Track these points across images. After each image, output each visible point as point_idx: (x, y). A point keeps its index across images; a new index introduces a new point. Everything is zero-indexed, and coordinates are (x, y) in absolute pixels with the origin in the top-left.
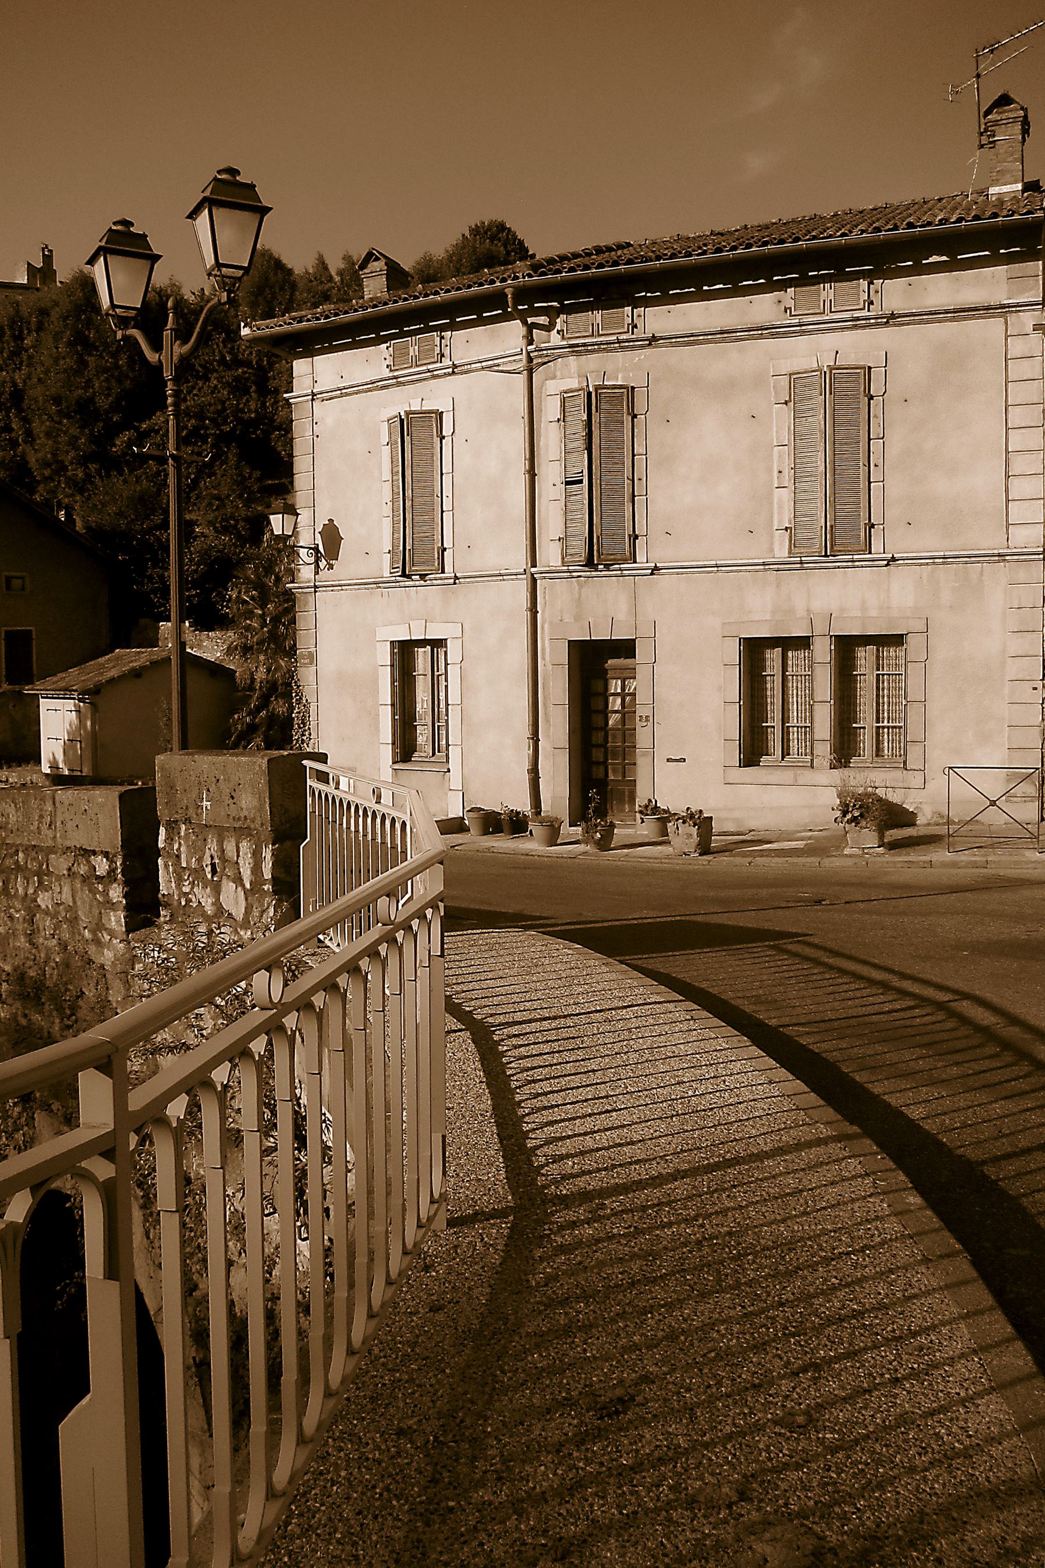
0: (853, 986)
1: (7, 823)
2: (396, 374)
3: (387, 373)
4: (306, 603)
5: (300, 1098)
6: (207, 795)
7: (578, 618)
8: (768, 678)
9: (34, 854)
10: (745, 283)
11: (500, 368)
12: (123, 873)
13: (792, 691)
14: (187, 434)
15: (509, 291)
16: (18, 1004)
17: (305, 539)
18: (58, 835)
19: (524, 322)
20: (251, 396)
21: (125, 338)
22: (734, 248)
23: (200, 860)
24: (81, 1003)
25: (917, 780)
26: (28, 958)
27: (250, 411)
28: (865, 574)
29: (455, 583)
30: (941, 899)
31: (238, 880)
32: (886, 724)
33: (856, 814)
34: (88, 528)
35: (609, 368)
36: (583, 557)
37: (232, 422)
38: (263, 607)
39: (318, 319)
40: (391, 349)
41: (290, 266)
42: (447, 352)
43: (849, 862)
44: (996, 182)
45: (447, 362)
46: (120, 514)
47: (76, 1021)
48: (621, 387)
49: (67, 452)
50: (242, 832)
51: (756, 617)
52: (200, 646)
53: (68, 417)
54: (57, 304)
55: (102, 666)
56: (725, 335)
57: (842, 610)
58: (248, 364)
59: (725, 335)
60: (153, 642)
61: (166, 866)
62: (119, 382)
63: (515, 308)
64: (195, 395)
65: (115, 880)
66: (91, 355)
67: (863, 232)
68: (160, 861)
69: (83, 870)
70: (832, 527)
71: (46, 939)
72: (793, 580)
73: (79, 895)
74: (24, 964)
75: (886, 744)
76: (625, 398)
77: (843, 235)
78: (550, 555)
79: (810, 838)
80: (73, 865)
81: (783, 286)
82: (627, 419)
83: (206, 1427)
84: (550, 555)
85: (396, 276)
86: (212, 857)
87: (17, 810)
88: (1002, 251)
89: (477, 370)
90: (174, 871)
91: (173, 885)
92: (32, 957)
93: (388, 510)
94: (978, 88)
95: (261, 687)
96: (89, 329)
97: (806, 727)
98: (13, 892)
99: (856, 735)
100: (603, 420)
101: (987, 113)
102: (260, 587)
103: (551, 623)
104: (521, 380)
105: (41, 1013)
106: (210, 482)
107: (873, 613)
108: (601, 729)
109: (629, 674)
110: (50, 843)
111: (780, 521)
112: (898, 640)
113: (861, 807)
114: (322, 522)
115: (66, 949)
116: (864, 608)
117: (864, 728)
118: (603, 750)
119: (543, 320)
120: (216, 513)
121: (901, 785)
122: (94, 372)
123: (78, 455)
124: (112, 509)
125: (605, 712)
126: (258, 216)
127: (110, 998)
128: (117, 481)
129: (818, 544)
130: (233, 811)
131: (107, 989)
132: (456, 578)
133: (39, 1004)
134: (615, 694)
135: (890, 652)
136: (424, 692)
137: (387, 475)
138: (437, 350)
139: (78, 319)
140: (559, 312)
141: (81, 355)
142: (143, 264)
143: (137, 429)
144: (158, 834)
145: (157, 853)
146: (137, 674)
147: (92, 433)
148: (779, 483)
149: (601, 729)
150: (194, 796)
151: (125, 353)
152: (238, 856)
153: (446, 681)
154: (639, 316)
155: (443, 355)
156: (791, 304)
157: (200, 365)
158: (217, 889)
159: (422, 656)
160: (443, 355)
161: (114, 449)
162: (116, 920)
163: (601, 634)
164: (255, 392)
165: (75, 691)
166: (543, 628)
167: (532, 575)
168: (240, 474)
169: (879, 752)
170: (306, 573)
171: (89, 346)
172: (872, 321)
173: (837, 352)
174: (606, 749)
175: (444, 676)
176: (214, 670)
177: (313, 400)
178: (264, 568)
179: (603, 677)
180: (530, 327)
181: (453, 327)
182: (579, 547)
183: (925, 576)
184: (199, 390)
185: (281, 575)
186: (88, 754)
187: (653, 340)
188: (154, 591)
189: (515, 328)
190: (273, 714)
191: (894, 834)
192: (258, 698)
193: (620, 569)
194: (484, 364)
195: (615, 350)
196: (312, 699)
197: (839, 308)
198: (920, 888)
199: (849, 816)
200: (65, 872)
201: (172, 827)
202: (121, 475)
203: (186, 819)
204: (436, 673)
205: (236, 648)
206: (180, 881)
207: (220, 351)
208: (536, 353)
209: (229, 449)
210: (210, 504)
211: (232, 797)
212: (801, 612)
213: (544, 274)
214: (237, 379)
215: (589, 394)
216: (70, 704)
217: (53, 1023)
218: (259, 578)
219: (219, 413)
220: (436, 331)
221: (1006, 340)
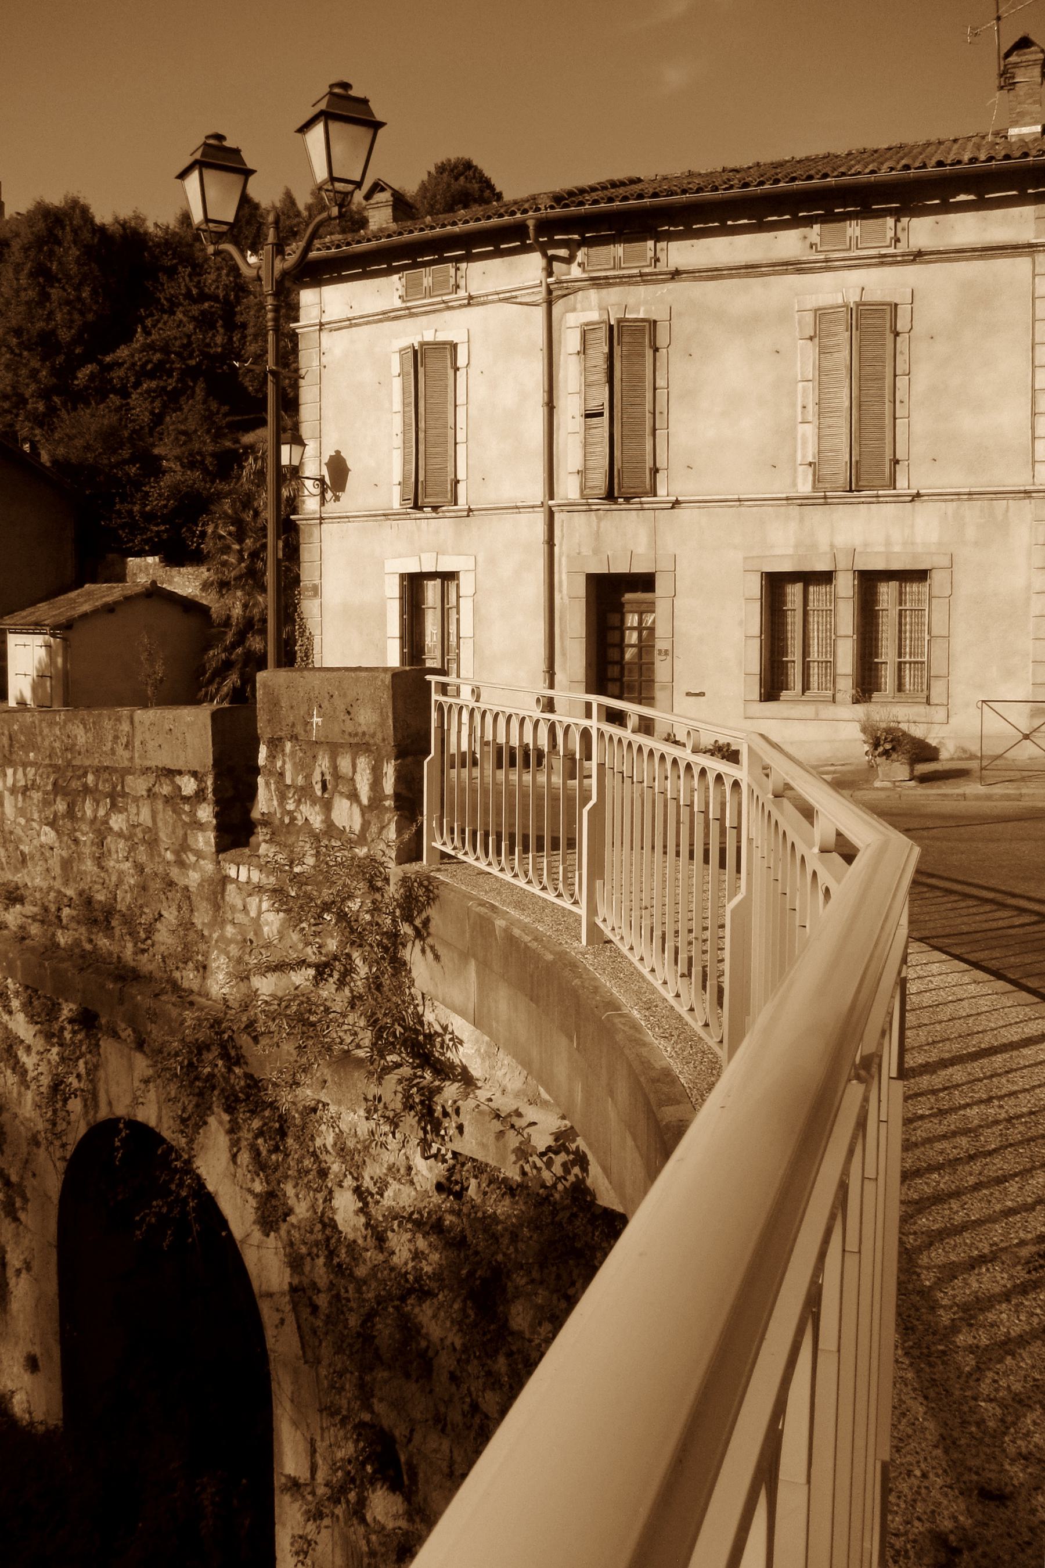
0: (963, 904)
1: (74, 745)
2: (409, 304)
3: (398, 303)
4: (311, 535)
5: (423, 1015)
6: (318, 711)
7: (596, 551)
8: (789, 613)
9: (106, 776)
10: (770, 219)
11: (518, 300)
12: (215, 791)
13: (813, 626)
14: (152, 368)
15: (531, 223)
16: (83, 930)
17: (311, 469)
18: (136, 755)
19: (544, 255)
20: (218, 331)
21: (217, 253)
22: (762, 183)
23: (308, 777)
24: (158, 925)
25: (939, 714)
26: (95, 882)
27: (216, 345)
28: (889, 509)
29: (468, 516)
30: (1000, 827)
31: (353, 796)
32: (907, 659)
33: (888, 746)
34: (55, 462)
35: (631, 301)
36: (602, 491)
37: (198, 356)
38: (241, 541)
39: (329, 248)
40: (404, 280)
41: (256, 200)
42: (462, 283)
43: (882, 795)
44: (1015, 123)
45: (462, 293)
46: (87, 448)
47: (153, 945)
48: (643, 320)
49: (27, 385)
50: (360, 746)
51: (778, 551)
52: (170, 582)
53: (30, 350)
54: (17, 235)
55: (74, 601)
56: (751, 270)
57: (866, 545)
58: (215, 298)
59: (751, 270)
60: (121, 578)
61: (267, 784)
62: (82, 313)
63: (536, 240)
64: (161, 329)
65: (204, 799)
66: (52, 286)
67: (892, 169)
68: (260, 780)
69: (166, 789)
70: (857, 462)
71: (118, 861)
72: (816, 515)
73: (160, 816)
74: (90, 888)
75: (907, 679)
76: (647, 332)
77: (873, 172)
78: (569, 488)
79: (834, 772)
80: (154, 785)
81: (809, 222)
82: (649, 353)
83: (301, 1353)
84: (569, 488)
85: (402, 206)
86: (323, 775)
87: (87, 731)
88: (1030, 191)
89: (493, 302)
90: (277, 789)
91: (275, 803)
92: (101, 881)
93: (398, 441)
94: (998, 30)
95: (237, 625)
96: (51, 262)
97: (827, 662)
98: (79, 815)
99: (877, 670)
100: (624, 353)
101: (1008, 55)
102: (238, 522)
103: (568, 556)
104: (540, 313)
105: (111, 937)
106: (177, 417)
107: (897, 549)
108: (616, 663)
109: (651, 607)
110: (126, 764)
111: (804, 456)
112: (921, 576)
113: (892, 741)
114: (328, 453)
115: (142, 870)
116: (888, 543)
117: (886, 663)
118: (618, 684)
119: (563, 252)
120: (183, 448)
121: (923, 720)
122: (55, 304)
123: (39, 388)
124: (79, 442)
125: (621, 646)
126: (371, 132)
127: (195, 921)
128: (85, 414)
129: (842, 479)
130: (349, 727)
131: (192, 911)
132: (470, 510)
133: (108, 929)
134: (632, 628)
135: (912, 588)
136: (433, 625)
137: (397, 406)
138: (452, 281)
139: (40, 250)
140: (580, 244)
141: (44, 287)
142: (236, 179)
143: (100, 363)
144: (258, 752)
145: (256, 771)
146: (110, 609)
147: (53, 367)
148: (803, 418)
149: (616, 663)
150: (302, 713)
151: (89, 285)
152: (354, 772)
153: (458, 613)
154: (662, 250)
155: (458, 287)
156: (816, 239)
157: (166, 299)
158: (327, 806)
159: (432, 590)
160: (458, 287)
161: (76, 382)
162: (205, 840)
163: (620, 567)
164: (222, 326)
165: (47, 625)
166: (560, 561)
167: (550, 508)
168: (208, 409)
169: (900, 688)
170: (310, 504)
171: (51, 278)
172: (899, 259)
173: (863, 289)
174: (622, 683)
175: (455, 610)
176: (188, 606)
177: (320, 330)
178: (242, 502)
179: (620, 610)
180: (550, 260)
181: (469, 258)
182: (599, 480)
183: (950, 512)
184: (165, 323)
185: (260, 509)
186: (60, 691)
187: (676, 274)
188: (123, 526)
189: (534, 262)
190: (249, 651)
191: (923, 768)
192: (234, 634)
193: (641, 503)
194: (502, 296)
195: (636, 283)
196: (316, 632)
197: (865, 245)
198: (963, 817)
199: (880, 749)
200: (145, 793)
201: (275, 744)
202: (88, 408)
203: (292, 736)
204: (446, 606)
205: (212, 584)
206: (282, 798)
207: (186, 285)
208: (556, 286)
209: (195, 384)
210: (177, 439)
211: (349, 713)
212: (824, 547)
213: (566, 206)
214: (203, 313)
215: (611, 327)
216: (39, 640)
217: (125, 947)
218: (236, 513)
219: (184, 346)
220: (451, 262)
221: (1034, 278)
